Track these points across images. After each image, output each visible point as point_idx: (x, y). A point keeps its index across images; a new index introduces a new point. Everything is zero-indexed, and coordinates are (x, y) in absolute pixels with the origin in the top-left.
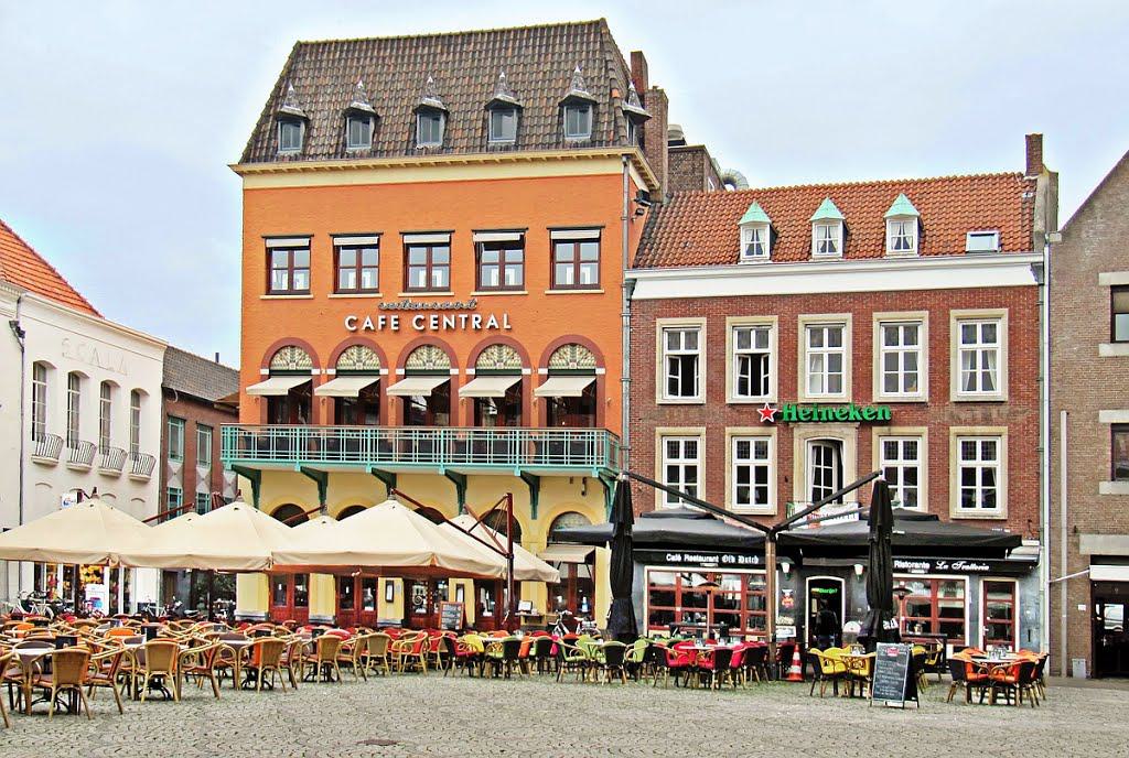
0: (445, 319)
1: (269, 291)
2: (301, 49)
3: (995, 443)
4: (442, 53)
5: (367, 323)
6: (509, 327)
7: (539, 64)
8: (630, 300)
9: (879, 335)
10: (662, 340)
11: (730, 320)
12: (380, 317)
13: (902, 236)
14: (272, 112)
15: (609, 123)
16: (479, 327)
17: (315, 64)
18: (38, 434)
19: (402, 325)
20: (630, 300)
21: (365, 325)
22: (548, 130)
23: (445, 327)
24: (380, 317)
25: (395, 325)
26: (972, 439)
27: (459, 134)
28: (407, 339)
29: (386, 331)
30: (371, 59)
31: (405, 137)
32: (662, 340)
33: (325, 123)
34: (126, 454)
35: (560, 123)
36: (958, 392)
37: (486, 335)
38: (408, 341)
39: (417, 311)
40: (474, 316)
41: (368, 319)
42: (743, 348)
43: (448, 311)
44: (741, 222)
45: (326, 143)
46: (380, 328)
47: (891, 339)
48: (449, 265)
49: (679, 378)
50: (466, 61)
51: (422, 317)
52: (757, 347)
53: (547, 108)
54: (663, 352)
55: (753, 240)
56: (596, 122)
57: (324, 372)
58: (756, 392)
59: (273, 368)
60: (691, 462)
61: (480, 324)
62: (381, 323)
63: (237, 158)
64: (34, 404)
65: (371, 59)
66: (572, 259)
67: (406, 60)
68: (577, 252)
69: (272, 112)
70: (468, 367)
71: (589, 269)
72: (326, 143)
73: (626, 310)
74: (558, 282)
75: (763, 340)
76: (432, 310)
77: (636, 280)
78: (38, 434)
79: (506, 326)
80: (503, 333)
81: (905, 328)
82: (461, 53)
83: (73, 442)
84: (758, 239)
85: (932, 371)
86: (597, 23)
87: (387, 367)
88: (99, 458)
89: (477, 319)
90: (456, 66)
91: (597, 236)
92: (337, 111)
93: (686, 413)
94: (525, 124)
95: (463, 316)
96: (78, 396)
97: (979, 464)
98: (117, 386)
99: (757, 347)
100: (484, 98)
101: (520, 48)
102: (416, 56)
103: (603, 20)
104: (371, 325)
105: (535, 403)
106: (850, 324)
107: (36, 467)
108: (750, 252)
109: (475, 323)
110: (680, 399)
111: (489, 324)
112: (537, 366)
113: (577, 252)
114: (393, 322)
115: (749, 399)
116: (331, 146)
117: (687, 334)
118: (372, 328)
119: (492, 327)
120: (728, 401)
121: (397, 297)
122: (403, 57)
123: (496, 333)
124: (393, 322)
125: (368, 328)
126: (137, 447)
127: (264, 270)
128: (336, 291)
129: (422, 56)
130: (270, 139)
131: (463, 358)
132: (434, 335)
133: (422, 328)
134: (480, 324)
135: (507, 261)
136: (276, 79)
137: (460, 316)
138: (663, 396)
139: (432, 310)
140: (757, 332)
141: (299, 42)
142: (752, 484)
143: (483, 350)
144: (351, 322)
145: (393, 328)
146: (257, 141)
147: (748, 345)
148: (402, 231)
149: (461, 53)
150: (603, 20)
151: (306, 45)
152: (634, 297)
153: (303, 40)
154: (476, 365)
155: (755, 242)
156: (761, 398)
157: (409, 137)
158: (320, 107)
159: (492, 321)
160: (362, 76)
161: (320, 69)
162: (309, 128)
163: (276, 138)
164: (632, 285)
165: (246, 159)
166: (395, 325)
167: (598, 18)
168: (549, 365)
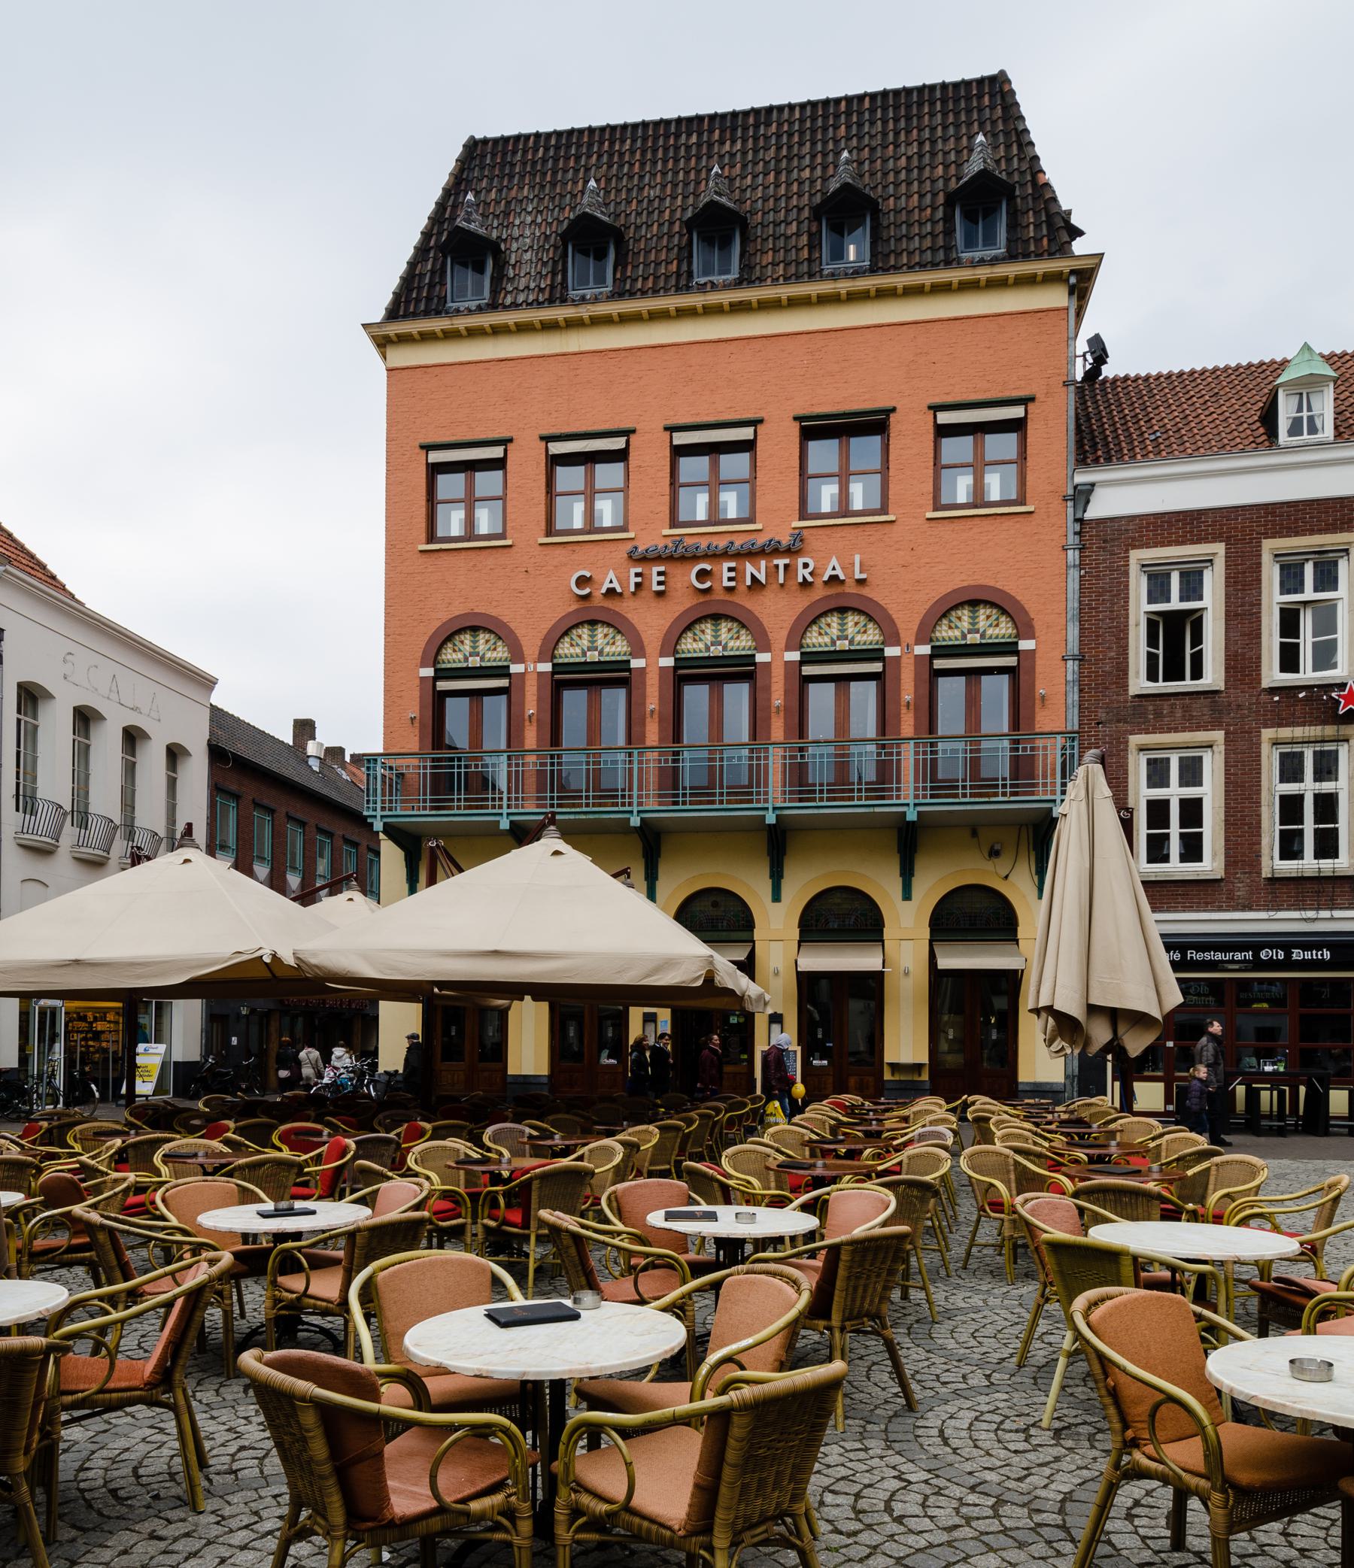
0: (750, 569)
1: (431, 537)
2: (476, 152)
3: (1201, 758)
4: (722, 142)
5: (610, 580)
6: (863, 576)
7: (897, 146)
8: (1080, 521)
9: (1271, 574)
10: (1139, 586)
11: (1269, 546)
12: (633, 571)
13: (1305, 414)
14: (432, 243)
15: (1037, 226)
16: (810, 579)
17: (502, 169)
18: (26, 800)
19: (672, 582)
20: (1080, 521)
21: (607, 585)
22: (928, 242)
23: (748, 582)
24: (633, 571)
25: (659, 583)
26: (1297, 749)
27: (769, 257)
28: (681, 603)
29: (643, 593)
30: (600, 156)
31: (674, 267)
32: (1139, 586)
33: (527, 256)
34: (116, 828)
35: (949, 232)
36: (1272, 675)
37: (819, 593)
38: (681, 609)
39: (696, 558)
40: (801, 561)
41: (611, 575)
42: (1289, 592)
43: (752, 554)
44: (1279, 381)
45: (532, 285)
46: (632, 589)
47: (1291, 580)
48: (503, 498)
49: (1160, 652)
50: (766, 149)
51: (708, 567)
52: (1182, 599)
53: (922, 210)
54: (1140, 606)
55: (1300, 409)
56: (1013, 226)
57: (531, 668)
58: (1174, 673)
59: (438, 666)
60: (1158, 793)
61: (811, 574)
62: (634, 580)
63: (378, 315)
64: (18, 753)
65: (600, 156)
66: (462, 496)
67: (660, 154)
68: (470, 486)
69: (432, 243)
70: (788, 648)
71: (734, 494)
72: (532, 285)
73: (1072, 539)
74: (560, 525)
75: (1192, 587)
76: (725, 555)
77: (1093, 485)
78: (26, 800)
79: (858, 576)
80: (850, 588)
81: (1182, 575)
82: (756, 139)
83: (81, 815)
84: (1309, 409)
85: (1255, 635)
86: (992, 79)
87: (643, 656)
88: (69, 833)
89: (806, 565)
90: (750, 157)
91: (501, 455)
92: (547, 238)
93: (1186, 709)
94: (885, 236)
95: (781, 562)
96: (36, 727)
97: (1174, 792)
98: (100, 718)
99: (1316, 590)
100: (806, 199)
101: (860, 125)
102: (677, 148)
103: (1002, 73)
104: (839, 572)
105: (652, 712)
106: (1220, 563)
107: (20, 851)
108: (1295, 429)
109: (802, 573)
110: (1162, 686)
111: (829, 572)
112: (911, 640)
113: (470, 486)
114: (656, 578)
115: (1162, 686)
116: (541, 290)
117: (1183, 575)
118: (619, 590)
119: (834, 578)
120: (1266, 683)
121: (657, 535)
122: (655, 151)
123: (839, 589)
124: (656, 578)
125: (611, 592)
126: (133, 819)
127: (424, 503)
128: (550, 531)
129: (688, 148)
130: (431, 286)
131: (779, 635)
132: (728, 597)
133: (587, 591)
134: (811, 574)
135: (478, 495)
136: (438, 193)
137: (776, 562)
138: (1139, 683)
139: (725, 555)
140: (1316, 565)
141: (472, 138)
142: (1175, 830)
143: (813, 618)
144: (582, 581)
145: (656, 588)
146: (411, 291)
147: (1299, 588)
148: (545, 432)
149: (756, 139)
150: (1002, 73)
151: (485, 141)
152: (1088, 515)
153: (479, 136)
154: (553, 657)
155: (1305, 414)
156: (1188, 684)
157: (679, 267)
158: (516, 232)
159: (833, 567)
160: (982, 125)
161: (511, 177)
162: (501, 265)
163: (443, 284)
164: (1083, 495)
165: (394, 313)
166: (659, 583)
167: (995, 72)
168: (801, 646)
